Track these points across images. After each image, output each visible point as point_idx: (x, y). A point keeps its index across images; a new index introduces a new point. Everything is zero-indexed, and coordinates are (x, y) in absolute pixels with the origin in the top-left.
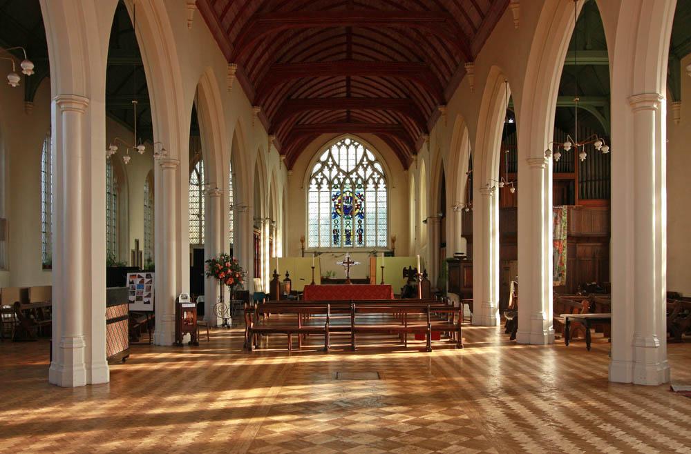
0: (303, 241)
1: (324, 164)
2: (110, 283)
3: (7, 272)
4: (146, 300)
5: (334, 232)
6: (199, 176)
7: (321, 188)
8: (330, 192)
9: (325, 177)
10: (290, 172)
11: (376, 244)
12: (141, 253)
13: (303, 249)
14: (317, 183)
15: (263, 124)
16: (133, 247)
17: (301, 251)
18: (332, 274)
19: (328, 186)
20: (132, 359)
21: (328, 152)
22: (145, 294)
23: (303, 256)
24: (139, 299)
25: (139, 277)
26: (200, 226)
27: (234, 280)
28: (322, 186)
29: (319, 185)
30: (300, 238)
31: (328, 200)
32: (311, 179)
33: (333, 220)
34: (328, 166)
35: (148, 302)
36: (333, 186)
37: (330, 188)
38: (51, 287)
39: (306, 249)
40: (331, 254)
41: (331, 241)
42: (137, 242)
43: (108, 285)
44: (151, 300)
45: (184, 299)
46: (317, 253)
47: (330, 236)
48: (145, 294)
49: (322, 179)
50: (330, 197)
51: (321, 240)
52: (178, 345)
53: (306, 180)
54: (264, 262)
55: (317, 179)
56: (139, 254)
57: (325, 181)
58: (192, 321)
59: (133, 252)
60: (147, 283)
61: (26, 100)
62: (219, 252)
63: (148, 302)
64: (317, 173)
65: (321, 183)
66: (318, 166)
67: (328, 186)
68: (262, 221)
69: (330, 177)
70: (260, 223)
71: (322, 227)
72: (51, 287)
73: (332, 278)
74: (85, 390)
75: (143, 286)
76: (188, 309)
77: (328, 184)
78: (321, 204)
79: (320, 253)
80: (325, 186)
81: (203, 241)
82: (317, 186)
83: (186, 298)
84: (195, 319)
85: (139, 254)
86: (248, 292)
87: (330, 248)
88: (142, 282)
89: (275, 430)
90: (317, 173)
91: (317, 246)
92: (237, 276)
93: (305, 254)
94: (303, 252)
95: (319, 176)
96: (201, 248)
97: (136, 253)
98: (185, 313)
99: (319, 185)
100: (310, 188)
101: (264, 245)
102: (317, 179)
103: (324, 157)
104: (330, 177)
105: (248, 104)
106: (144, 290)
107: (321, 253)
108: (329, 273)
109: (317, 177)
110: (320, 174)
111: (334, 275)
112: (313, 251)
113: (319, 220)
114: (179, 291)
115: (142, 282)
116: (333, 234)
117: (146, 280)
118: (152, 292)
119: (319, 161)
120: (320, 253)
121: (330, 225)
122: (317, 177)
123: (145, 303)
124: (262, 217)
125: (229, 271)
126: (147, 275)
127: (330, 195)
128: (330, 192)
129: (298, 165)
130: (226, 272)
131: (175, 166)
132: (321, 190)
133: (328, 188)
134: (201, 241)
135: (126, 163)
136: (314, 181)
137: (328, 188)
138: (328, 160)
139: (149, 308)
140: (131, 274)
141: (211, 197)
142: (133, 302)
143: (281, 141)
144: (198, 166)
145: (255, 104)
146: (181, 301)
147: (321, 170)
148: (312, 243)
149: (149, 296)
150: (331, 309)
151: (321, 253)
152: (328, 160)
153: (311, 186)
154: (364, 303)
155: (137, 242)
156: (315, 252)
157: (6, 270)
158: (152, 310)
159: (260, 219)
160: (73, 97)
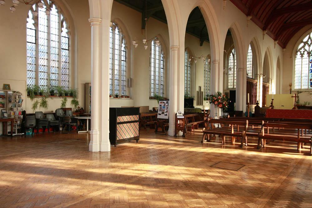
0: (291, 85)
1: (306, 43)
2: (186, 106)
3: (131, 100)
4: (165, 114)
5: (311, 80)
6: (233, 55)
7: (303, 56)
8: (309, 58)
9: (306, 50)
10: (284, 50)
11: (301, 87)
12: (202, 92)
13: (291, 90)
14: (301, 54)
15: (257, 25)
16: (197, 89)
17: (290, 91)
18: (307, 104)
19: (308, 55)
20: (141, 141)
21: (308, 36)
22: (166, 111)
23: (290, 94)
24: (163, 113)
25: (164, 103)
26: (234, 80)
27: (222, 105)
28: (304, 55)
29: (302, 55)
30: (288, 84)
31: (308, 63)
32: (297, 52)
33: (310, 74)
34: (308, 44)
35: (166, 115)
36: (311, 55)
37: (309, 56)
38: (149, 106)
39: (293, 90)
40: (308, 92)
41: (308, 85)
42: (200, 87)
43: (185, 107)
44: (167, 113)
45: (180, 114)
46: (299, 92)
47: (308, 82)
48: (166, 111)
49: (304, 52)
50: (309, 61)
51: (302, 85)
52: (176, 136)
53: (294, 52)
54: (259, 96)
55: (300, 52)
56: (201, 93)
57: (306, 53)
58: (183, 125)
59: (198, 92)
60: (167, 106)
61: (142, 29)
62: (217, 91)
63: (166, 115)
64: (301, 49)
65: (304, 54)
66: (302, 44)
67: (308, 55)
68: (258, 76)
69: (309, 50)
70: (257, 76)
71: (303, 78)
72: (149, 106)
73: (307, 105)
74: (98, 154)
75: (165, 107)
76: (180, 119)
77: (307, 54)
78: (302, 66)
79: (301, 92)
80: (306, 55)
81: (235, 87)
82: (301, 56)
83: (181, 113)
84: (184, 124)
85: (201, 93)
86: (242, 112)
87: (300, 89)
88: (164, 105)
89: (247, 181)
90: (301, 49)
91: (300, 88)
92: (224, 103)
93: (292, 93)
94: (291, 92)
95: (302, 50)
96: (234, 90)
97: (199, 92)
98: (179, 121)
99: (302, 55)
100: (296, 57)
101: (259, 88)
102: (300, 52)
103: (305, 40)
104: (309, 50)
105: (244, 16)
106: (165, 109)
107: (302, 92)
108: (306, 103)
109: (301, 51)
110: (303, 49)
111: (309, 104)
112: (297, 91)
113: (301, 74)
114: (178, 109)
115: (164, 105)
116: (310, 81)
117: (166, 104)
118: (168, 110)
119: (302, 42)
120: (301, 92)
121: (309, 76)
122: (301, 51)
123: (165, 115)
124: (258, 73)
125: (220, 101)
126: (167, 102)
127: (309, 60)
128: (309, 58)
129: (289, 46)
130: (218, 101)
131: (177, 49)
132: (303, 58)
133: (308, 56)
134: (234, 87)
135: (146, 49)
136: (299, 53)
137: (308, 56)
138: (308, 41)
139: (166, 117)
140: (161, 101)
141: (213, 64)
142: (160, 114)
143: (274, 33)
144: (233, 51)
145: (248, 15)
146: (178, 115)
147: (303, 47)
148: (297, 86)
149: (167, 112)
150: (249, 123)
151: (302, 92)
152: (308, 41)
153: (297, 56)
154: (290, 121)
155: (200, 87)
156: (298, 92)
157: (132, 99)
158: (168, 118)
159: (257, 74)
160: (93, 19)
